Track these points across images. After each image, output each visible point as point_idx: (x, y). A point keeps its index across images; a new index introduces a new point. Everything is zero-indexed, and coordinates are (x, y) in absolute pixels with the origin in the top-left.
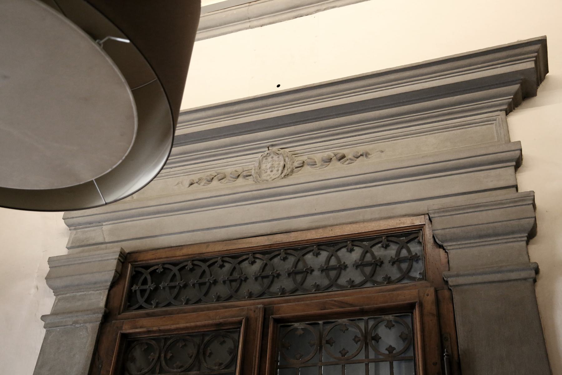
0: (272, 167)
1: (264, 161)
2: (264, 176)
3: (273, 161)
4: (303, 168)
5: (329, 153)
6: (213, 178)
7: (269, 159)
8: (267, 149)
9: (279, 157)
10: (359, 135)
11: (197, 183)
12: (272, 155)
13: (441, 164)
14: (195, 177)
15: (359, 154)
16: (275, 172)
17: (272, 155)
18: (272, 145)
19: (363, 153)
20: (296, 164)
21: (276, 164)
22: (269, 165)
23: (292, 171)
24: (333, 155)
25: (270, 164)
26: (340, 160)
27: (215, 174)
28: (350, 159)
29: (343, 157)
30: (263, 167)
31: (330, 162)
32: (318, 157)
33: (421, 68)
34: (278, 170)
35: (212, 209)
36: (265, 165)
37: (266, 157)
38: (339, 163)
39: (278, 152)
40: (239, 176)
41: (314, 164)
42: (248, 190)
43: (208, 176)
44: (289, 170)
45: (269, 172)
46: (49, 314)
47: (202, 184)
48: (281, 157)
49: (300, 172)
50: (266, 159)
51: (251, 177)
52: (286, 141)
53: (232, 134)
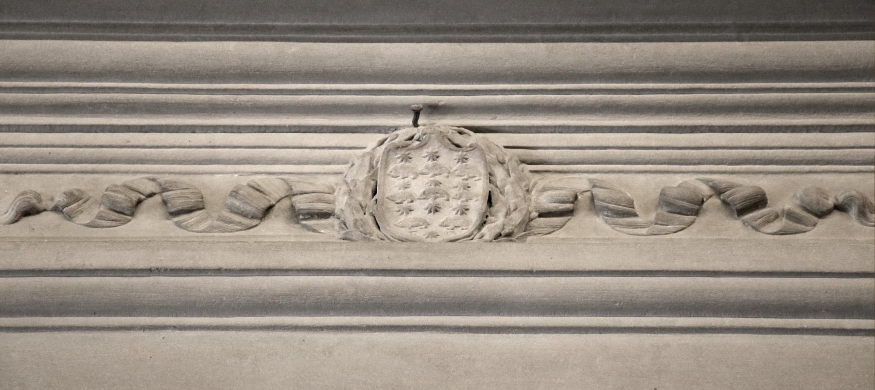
0: (435, 191)
1: (396, 163)
2: (398, 224)
3: (438, 170)
4: (573, 222)
5: (691, 179)
6: (139, 202)
7: (421, 161)
8: (409, 121)
9: (464, 159)
10: (822, 129)
11: (56, 209)
12: (434, 146)
14: (54, 187)
15: (831, 202)
16: (449, 213)
17: (434, 146)
18: (434, 109)
19: (850, 200)
20: (545, 201)
22: (418, 186)
23: (526, 225)
24: (705, 190)
25: (426, 179)
26: (742, 212)
27: (150, 187)
28: (790, 215)
29: (757, 202)
30: (392, 186)
31: (696, 213)
32: (642, 186)
33: (727, 127)
34: (464, 211)
35: (144, 328)
36: (399, 182)
37: (405, 149)
38: (736, 227)
39: (459, 139)
40: (270, 208)
41: (623, 212)
42: (336, 264)
43: (114, 188)
45: (420, 210)
47: (84, 218)
48: (474, 161)
49: (560, 234)
50: (406, 158)
51: (331, 220)
52: (499, 98)
53: (255, 29)
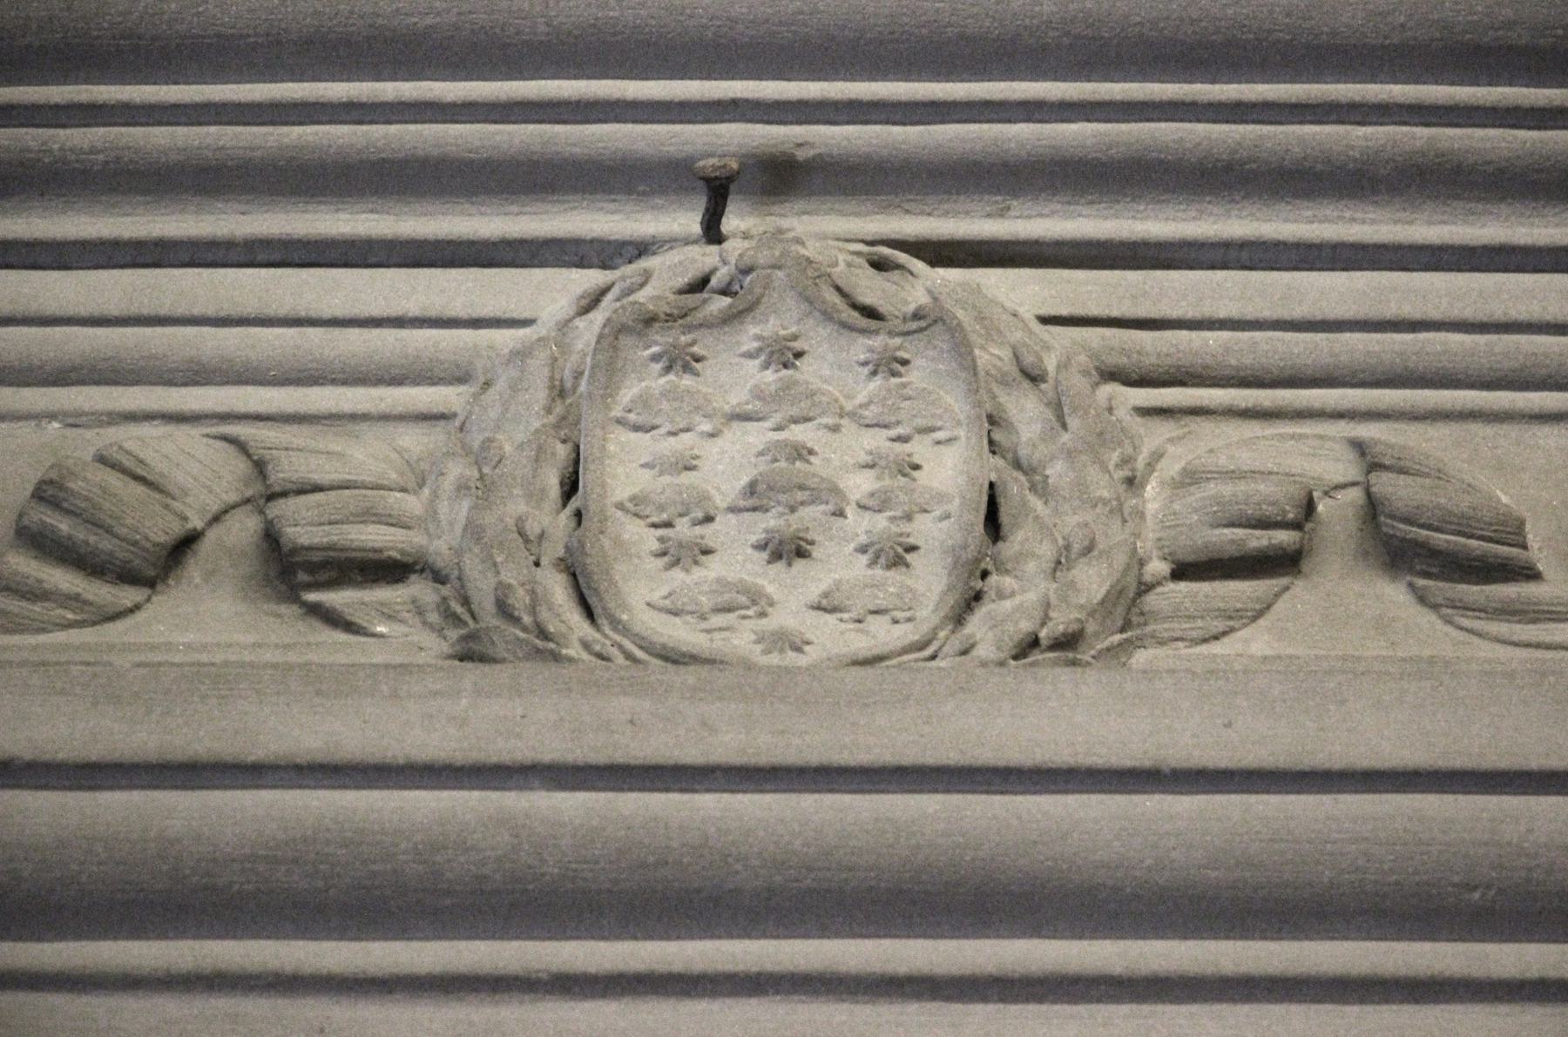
7: (733, 371)
8: (689, 221)
9: (891, 365)
13: (1151, 804)
16: (839, 564)
21: (844, 457)
22: (727, 463)
23: (1128, 605)
39: (871, 287)
44: (1092, 581)
45: (736, 555)
46: (571, 313)
52: (1020, 134)
